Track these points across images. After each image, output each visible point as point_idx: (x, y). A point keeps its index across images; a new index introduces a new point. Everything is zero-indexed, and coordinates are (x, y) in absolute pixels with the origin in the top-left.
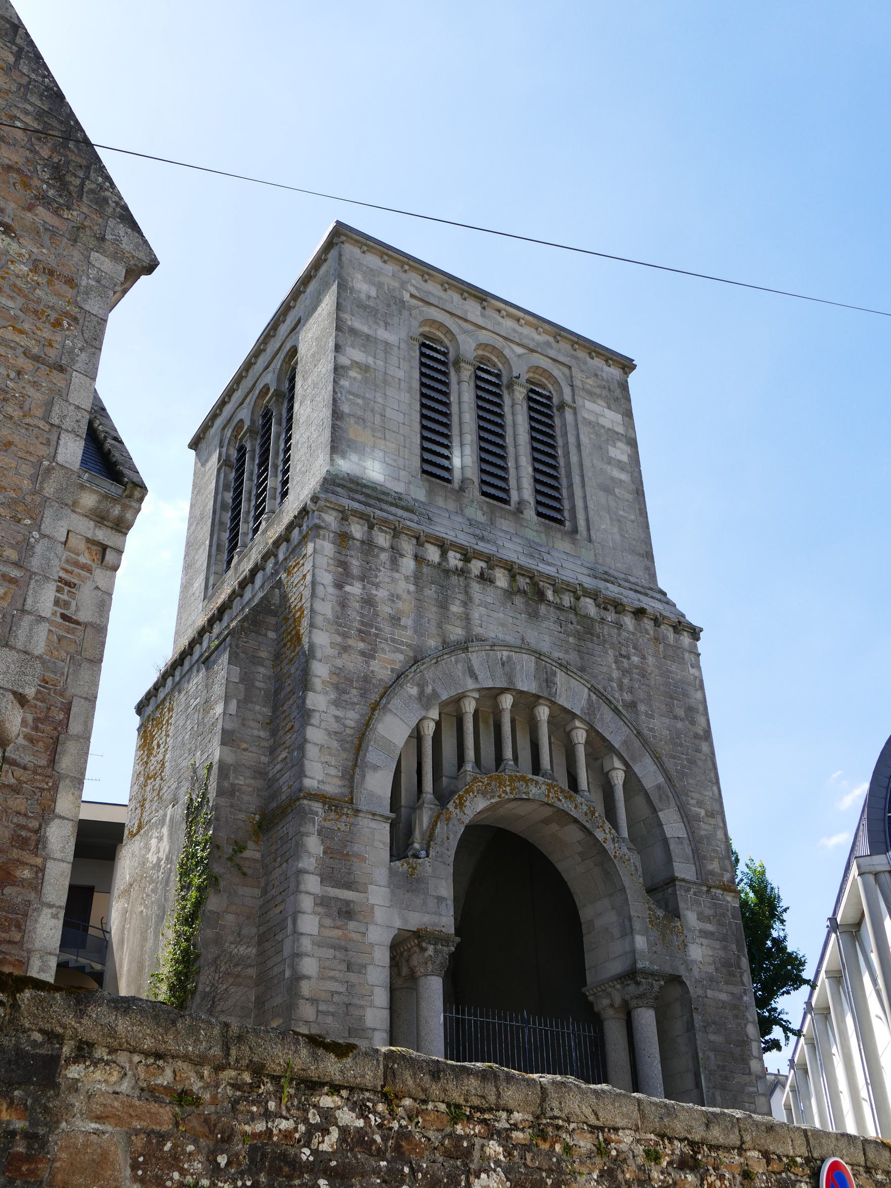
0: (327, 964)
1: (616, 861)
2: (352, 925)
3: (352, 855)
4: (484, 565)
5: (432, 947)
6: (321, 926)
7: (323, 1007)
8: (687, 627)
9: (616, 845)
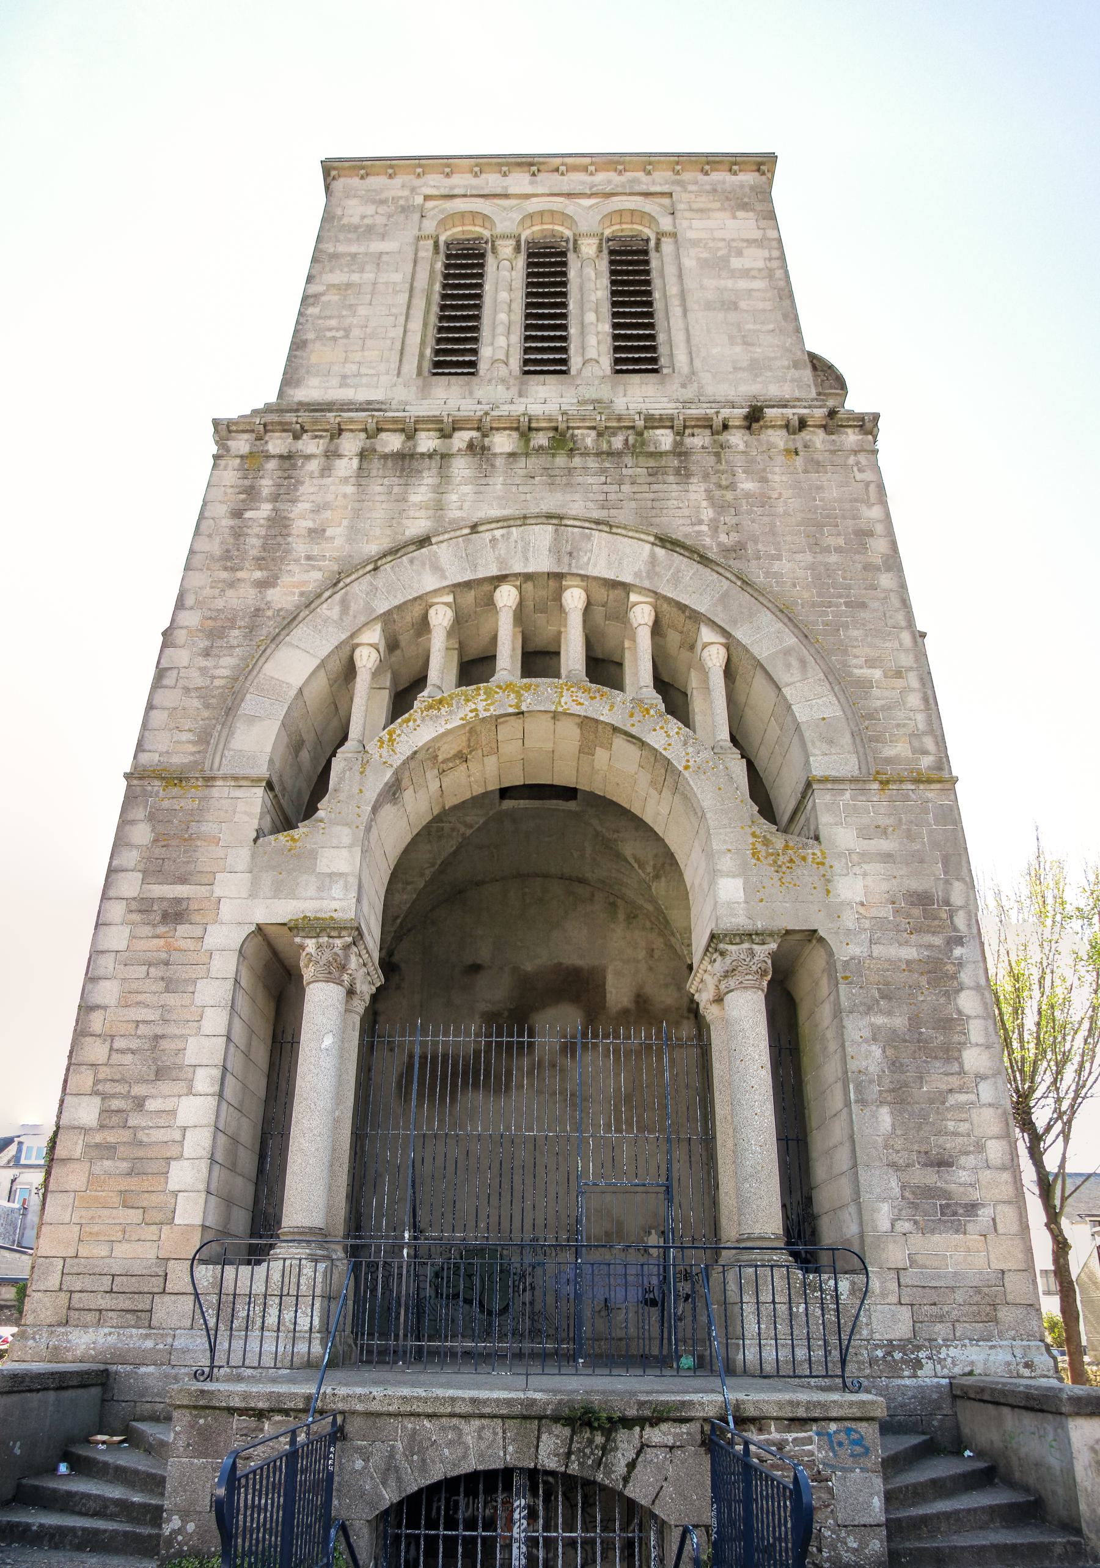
0: (134, 986)
2: (182, 930)
3: (198, 838)
4: (474, 434)
5: (314, 940)
6: (133, 937)
7: (119, 1043)
9: (690, 750)
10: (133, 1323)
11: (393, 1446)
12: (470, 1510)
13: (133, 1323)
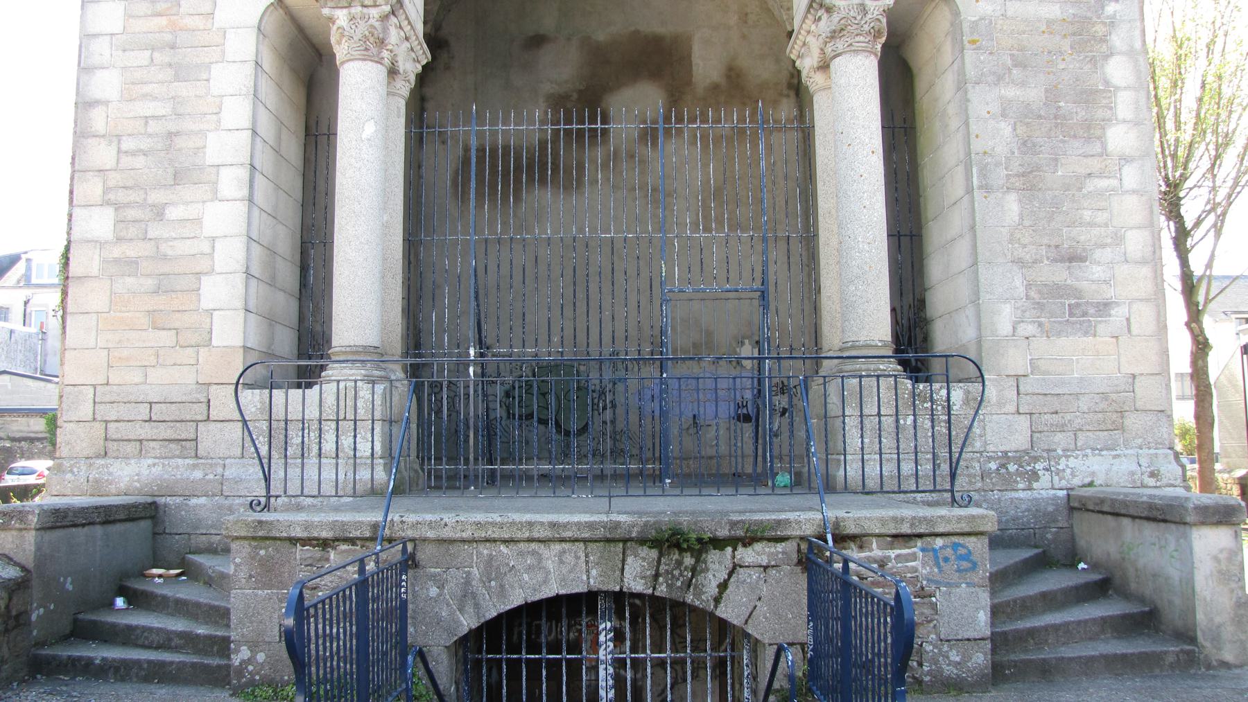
10: (177, 453)
11: (469, 573)
12: (553, 634)
13: (177, 453)
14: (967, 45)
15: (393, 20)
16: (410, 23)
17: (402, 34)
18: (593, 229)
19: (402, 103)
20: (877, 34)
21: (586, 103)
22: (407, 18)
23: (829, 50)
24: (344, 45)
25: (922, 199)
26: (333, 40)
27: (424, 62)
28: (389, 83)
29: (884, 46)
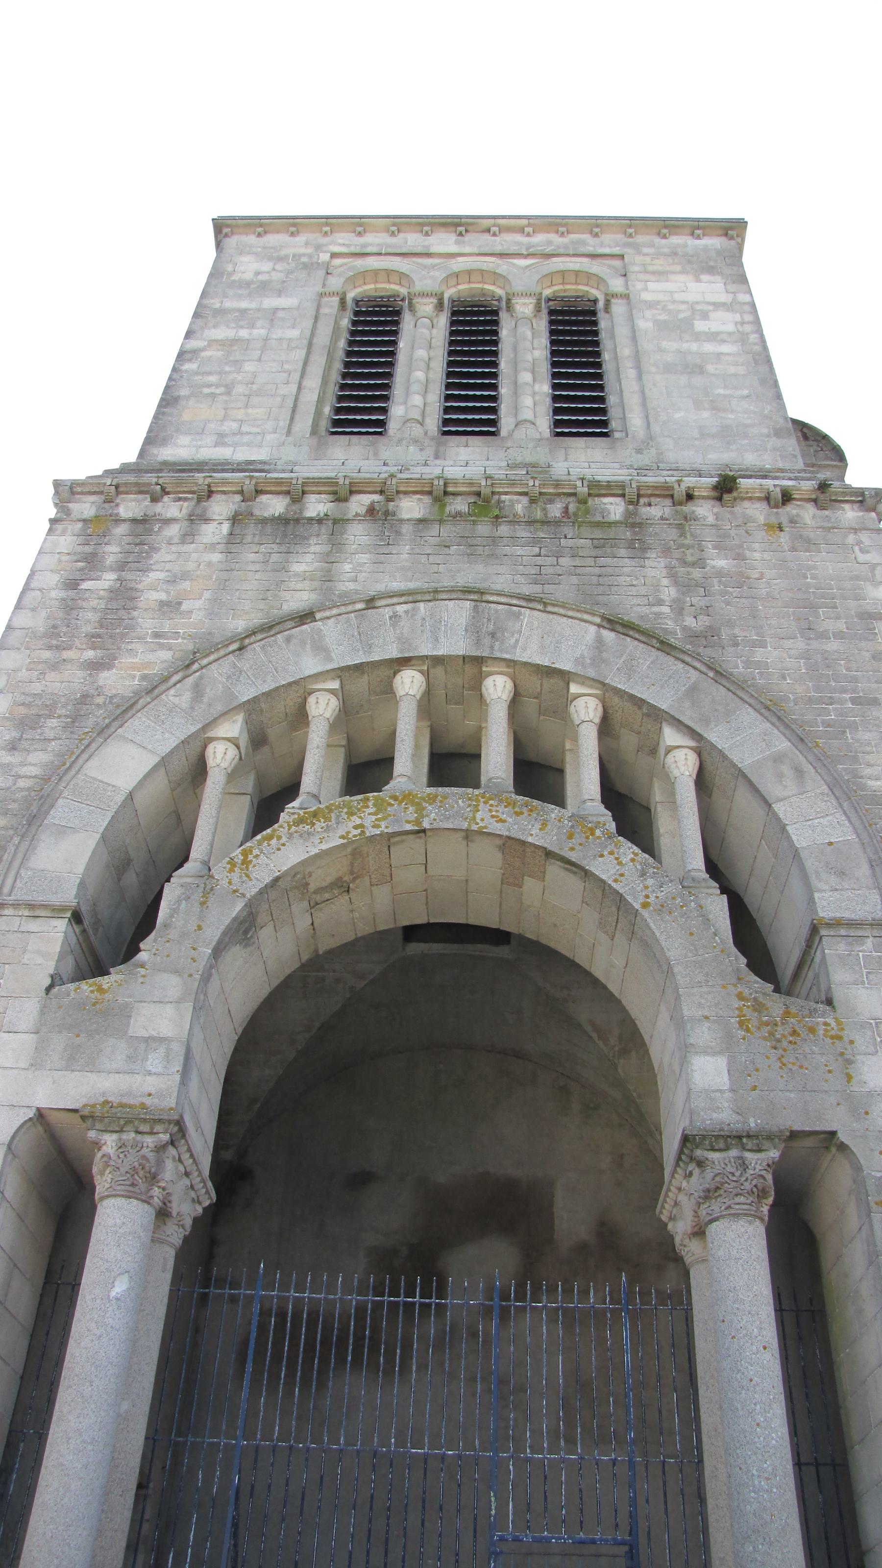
1: (645, 913)
8: (845, 494)
14: (874, 1207)
15: (172, 1151)
16: (192, 1156)
17: (181, 1168)
18: (401, 1443)
19: (170, 1254)
20: (762, 1194)
21: (418, 1264)
22: (189, 1150)
23: (703, 1212)
24: (108, 1177)
25: (842, 1411)
26: (95, 1170)
27: (207, 1203)
28: (157, 1228)
29: (773, 1206)
